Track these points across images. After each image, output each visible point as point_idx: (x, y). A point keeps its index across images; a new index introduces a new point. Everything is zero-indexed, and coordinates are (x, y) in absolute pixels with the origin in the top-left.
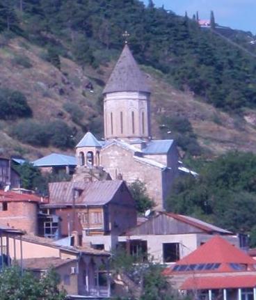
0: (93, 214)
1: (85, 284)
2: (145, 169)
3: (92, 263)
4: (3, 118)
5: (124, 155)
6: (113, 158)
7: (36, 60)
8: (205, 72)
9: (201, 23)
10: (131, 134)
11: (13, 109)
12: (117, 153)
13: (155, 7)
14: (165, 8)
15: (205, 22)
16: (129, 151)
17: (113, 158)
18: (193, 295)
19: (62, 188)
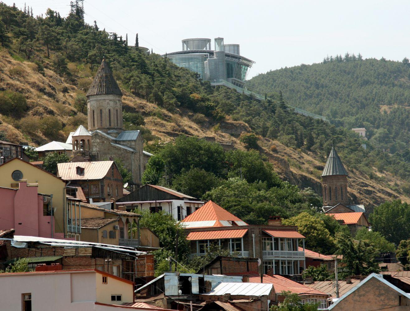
0: (92, 186)
1: (38, 243)
2: (120, 153)
3: (127, 221)
4: (3, 114)
5: (103, 142)
6: (96, 144)
7: (29, 70)
8: (145, 80)
9: (62, 17)
10: (108, 126)
11: (16, 109)
12: (98, 140)
13: (99, 30)
14: (106, 31)
15: (131, 43)
16: (107, 139)
17: (96, 144)
18: (314, 213)
19: (68, 167)
